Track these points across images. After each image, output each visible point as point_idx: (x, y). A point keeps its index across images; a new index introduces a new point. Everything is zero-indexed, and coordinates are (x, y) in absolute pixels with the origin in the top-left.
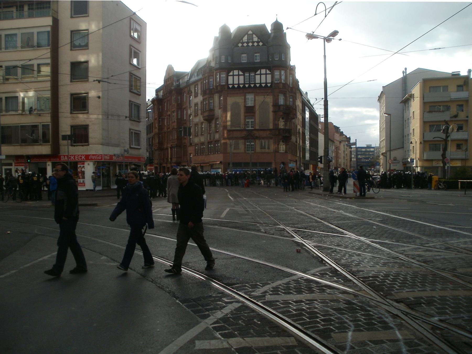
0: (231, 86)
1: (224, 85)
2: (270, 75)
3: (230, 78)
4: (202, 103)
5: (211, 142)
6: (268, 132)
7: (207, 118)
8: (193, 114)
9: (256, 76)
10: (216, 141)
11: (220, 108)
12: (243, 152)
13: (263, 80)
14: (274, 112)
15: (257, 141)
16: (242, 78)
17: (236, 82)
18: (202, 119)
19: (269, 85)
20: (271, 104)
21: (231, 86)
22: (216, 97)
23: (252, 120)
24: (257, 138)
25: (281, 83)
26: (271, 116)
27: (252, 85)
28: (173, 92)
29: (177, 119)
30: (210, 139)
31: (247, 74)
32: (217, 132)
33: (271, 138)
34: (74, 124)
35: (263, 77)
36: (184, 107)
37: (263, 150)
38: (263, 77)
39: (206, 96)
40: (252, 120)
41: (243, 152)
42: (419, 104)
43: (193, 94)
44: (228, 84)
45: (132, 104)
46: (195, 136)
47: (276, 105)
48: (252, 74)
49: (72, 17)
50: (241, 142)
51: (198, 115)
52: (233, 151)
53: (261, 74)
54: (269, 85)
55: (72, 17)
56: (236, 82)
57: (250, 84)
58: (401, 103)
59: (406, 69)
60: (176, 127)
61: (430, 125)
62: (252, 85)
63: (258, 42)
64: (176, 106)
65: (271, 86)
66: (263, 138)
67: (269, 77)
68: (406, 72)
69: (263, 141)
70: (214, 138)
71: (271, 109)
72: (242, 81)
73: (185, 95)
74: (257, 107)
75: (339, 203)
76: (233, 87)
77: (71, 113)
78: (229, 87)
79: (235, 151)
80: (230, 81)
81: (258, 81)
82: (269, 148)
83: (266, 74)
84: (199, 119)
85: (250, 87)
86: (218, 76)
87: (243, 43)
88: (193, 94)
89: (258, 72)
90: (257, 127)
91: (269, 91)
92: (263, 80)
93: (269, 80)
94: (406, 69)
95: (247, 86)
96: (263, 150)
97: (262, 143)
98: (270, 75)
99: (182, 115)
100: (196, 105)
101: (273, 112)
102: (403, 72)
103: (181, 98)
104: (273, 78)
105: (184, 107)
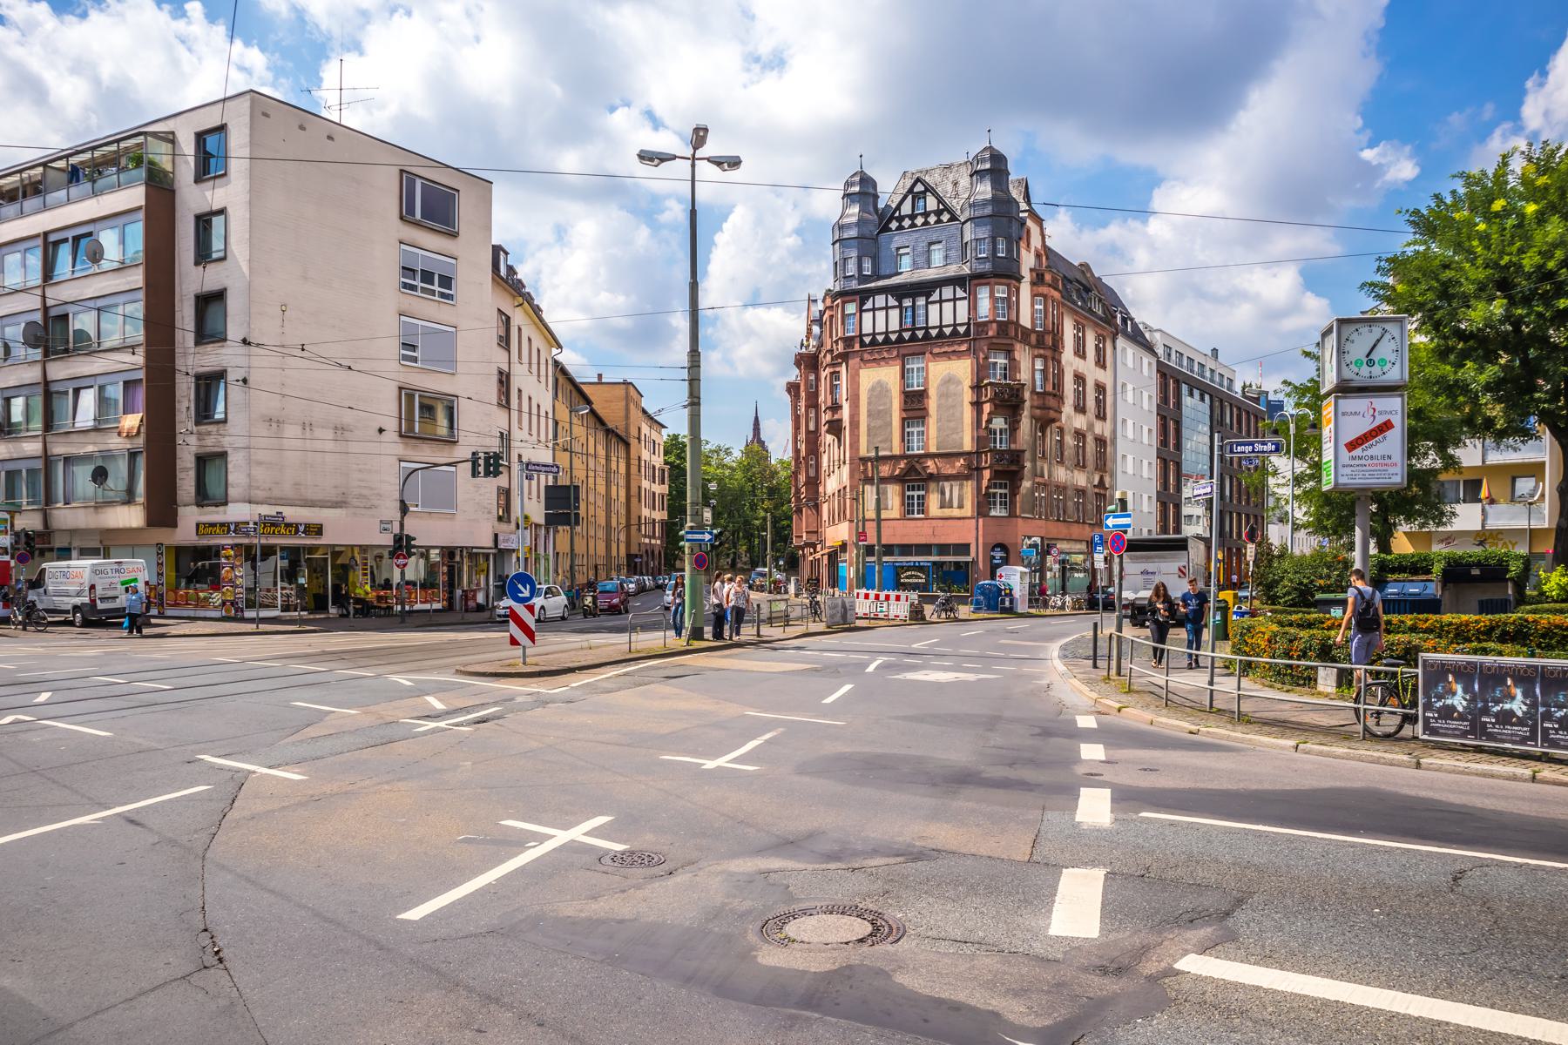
9: (865, 315)
16: (894, 314)
17: (881, 327)
19: (962, 330)
20: (967, 382)
31: (907, 303)
33: (967, 478)
34: (202, 450)
35: (881, 315)
37: (947, 512)
38: (948, 307)
45: (410, 397)
54: (962, 330)
61: (125, 383)
65: (967, 333)
66: (948, 478)
67: (962, 306)
69: (947, 485)
71: (968, 396)
72: (894, 325)
74: (932, 392)
77: (197, 423)
81: (934, 320)
82: (961, 506)
83: (887, 308)
85: (913, 338)
89: (935, 297)
90: (933, 450)
91: (964, 347)
93: (962, 317)
96: (947, 512)
98: (897, 311)
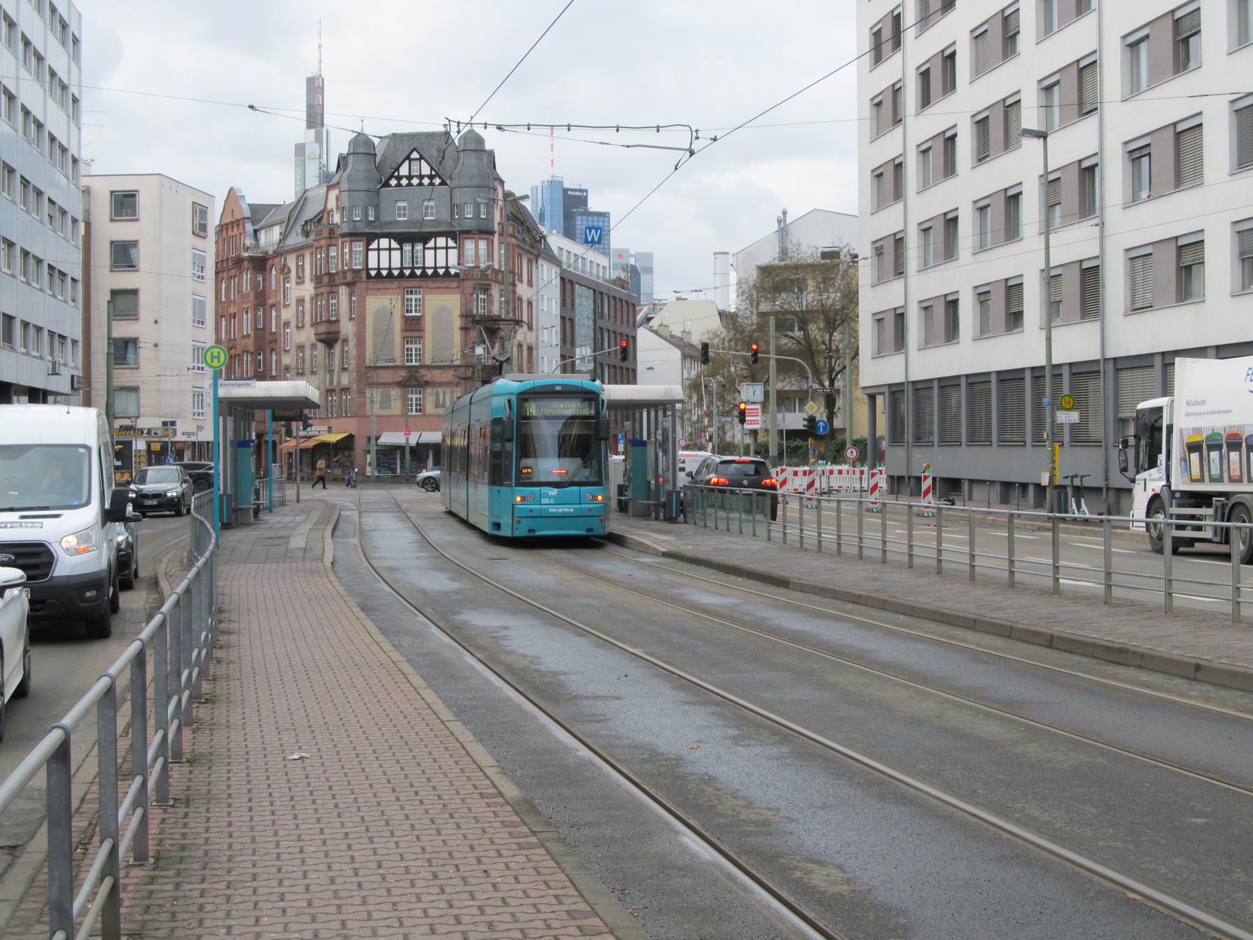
0: (373, 273)
1: (359, 271)
2: (455, 251)
3: (373, 256)
4: (315, 298)
5: (334, 390)
6: (451, 372)
7: (323, 337)
8: (293, 324)
10: (342, 390)
11: (351, 319)
12: (399, 413)
13: (441, 262)
14: (465, 329)
15: (429, 390)
16: (396, 255)
17: (384, 264)
18: (313, 338)
21: (373, 273)
22: (343, 291)
23: (418, 346)
24: (427, 383)
25: (477, 267)
26: (457, 336)
27: (418, 272)
28: (246, 263)
29: (256, 330)
30: (331, 383)
31: (407, 247)
32: (344, 369)
36: (270, 302)
39: (323, 290)
40: (418, 346)
41: (399, 413)
42: (1228, 154)
43: (293, 275)
44: (368, 269)
46: (298, 328)
47: (467, 316)
48: (419, 247)
49: (112, 220)
50: (395, 392)
51: (303, 326)
52: (377, 410)
53: (435, 248)
55: (112, 220)
56: (384, 264)
57: (413, 268)
58: (722, 314)
59: (785, 213)
60: (251, 349)
62: (418, 272)
63: (431, 177)
64: (252, 297)
66: (441, 385)
67: (453, 254)
68: (785, 220)
69: (441, 390)
70: (339, 383)
71: (457, 323)
72: (396, 263)
73: (274, 272)
75: (728, 538)
76: (379, 275)
78: (369, 276)
79: (383, 412)
80: (373, 263)
84: (307, 336)
86: (346, 250)
87: (399, 178)
88: (293, 275)
89: (431, 244)
90: (428, 362)
92: (441, 262)
94: (785, 213)
95: (407, 272)
97: (437, 394)
98: (455, 251)
99: (267, 317)
100: (300, 301)
101: (461, 329)
102: (779, 221)
103: (264, 280)
104: (460, 256)
105: (270, 302)
